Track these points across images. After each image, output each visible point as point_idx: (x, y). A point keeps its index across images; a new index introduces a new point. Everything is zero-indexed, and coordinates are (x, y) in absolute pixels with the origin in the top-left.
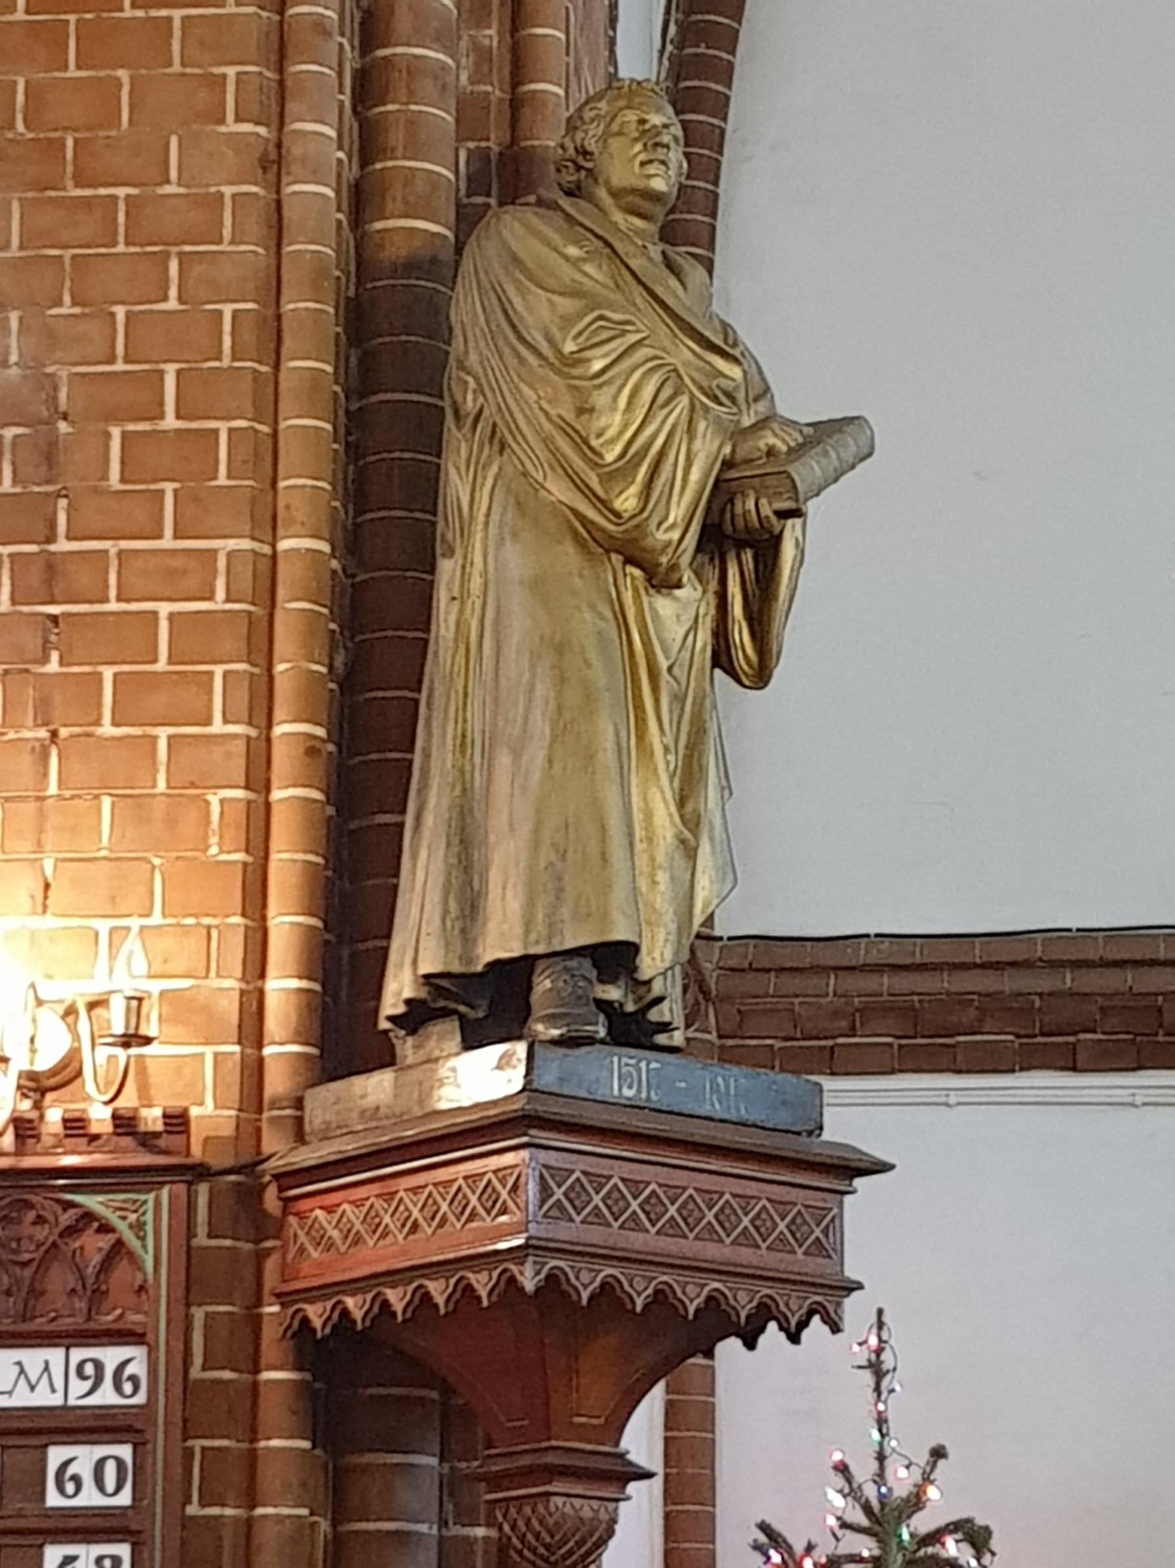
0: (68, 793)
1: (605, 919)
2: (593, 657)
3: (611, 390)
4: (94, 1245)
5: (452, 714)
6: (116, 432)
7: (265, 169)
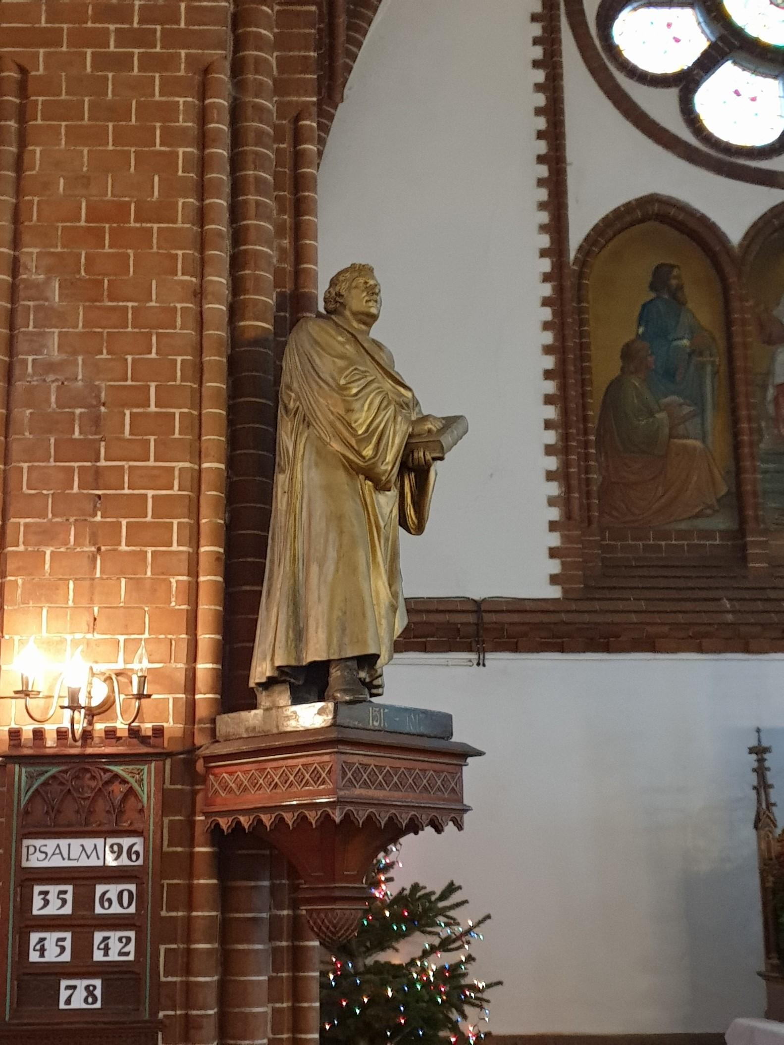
0: (105, 577)
1: (365, 643)
2: (355, 522)
3: (361, 402)
4: (118, 789)
5: (288, 546)
6: (128, 412)
7: (195, 296)
